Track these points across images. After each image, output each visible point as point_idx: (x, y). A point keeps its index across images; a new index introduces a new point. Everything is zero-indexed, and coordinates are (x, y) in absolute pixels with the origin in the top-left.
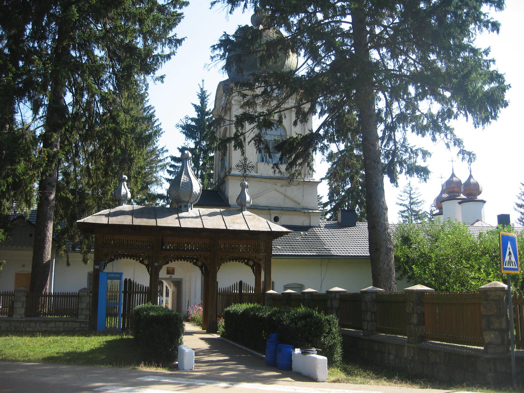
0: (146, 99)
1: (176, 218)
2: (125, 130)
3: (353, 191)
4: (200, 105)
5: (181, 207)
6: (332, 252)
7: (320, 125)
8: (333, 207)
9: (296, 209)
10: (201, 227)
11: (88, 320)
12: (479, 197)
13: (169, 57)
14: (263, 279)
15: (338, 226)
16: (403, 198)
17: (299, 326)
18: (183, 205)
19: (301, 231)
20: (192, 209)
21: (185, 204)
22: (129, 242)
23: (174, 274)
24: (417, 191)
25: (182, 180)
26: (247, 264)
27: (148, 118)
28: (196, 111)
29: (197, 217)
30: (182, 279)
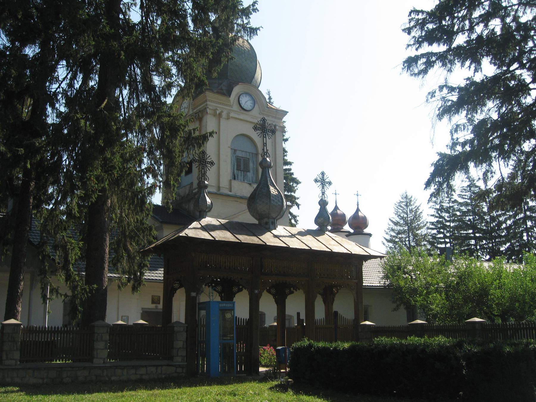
12: (366, 231)
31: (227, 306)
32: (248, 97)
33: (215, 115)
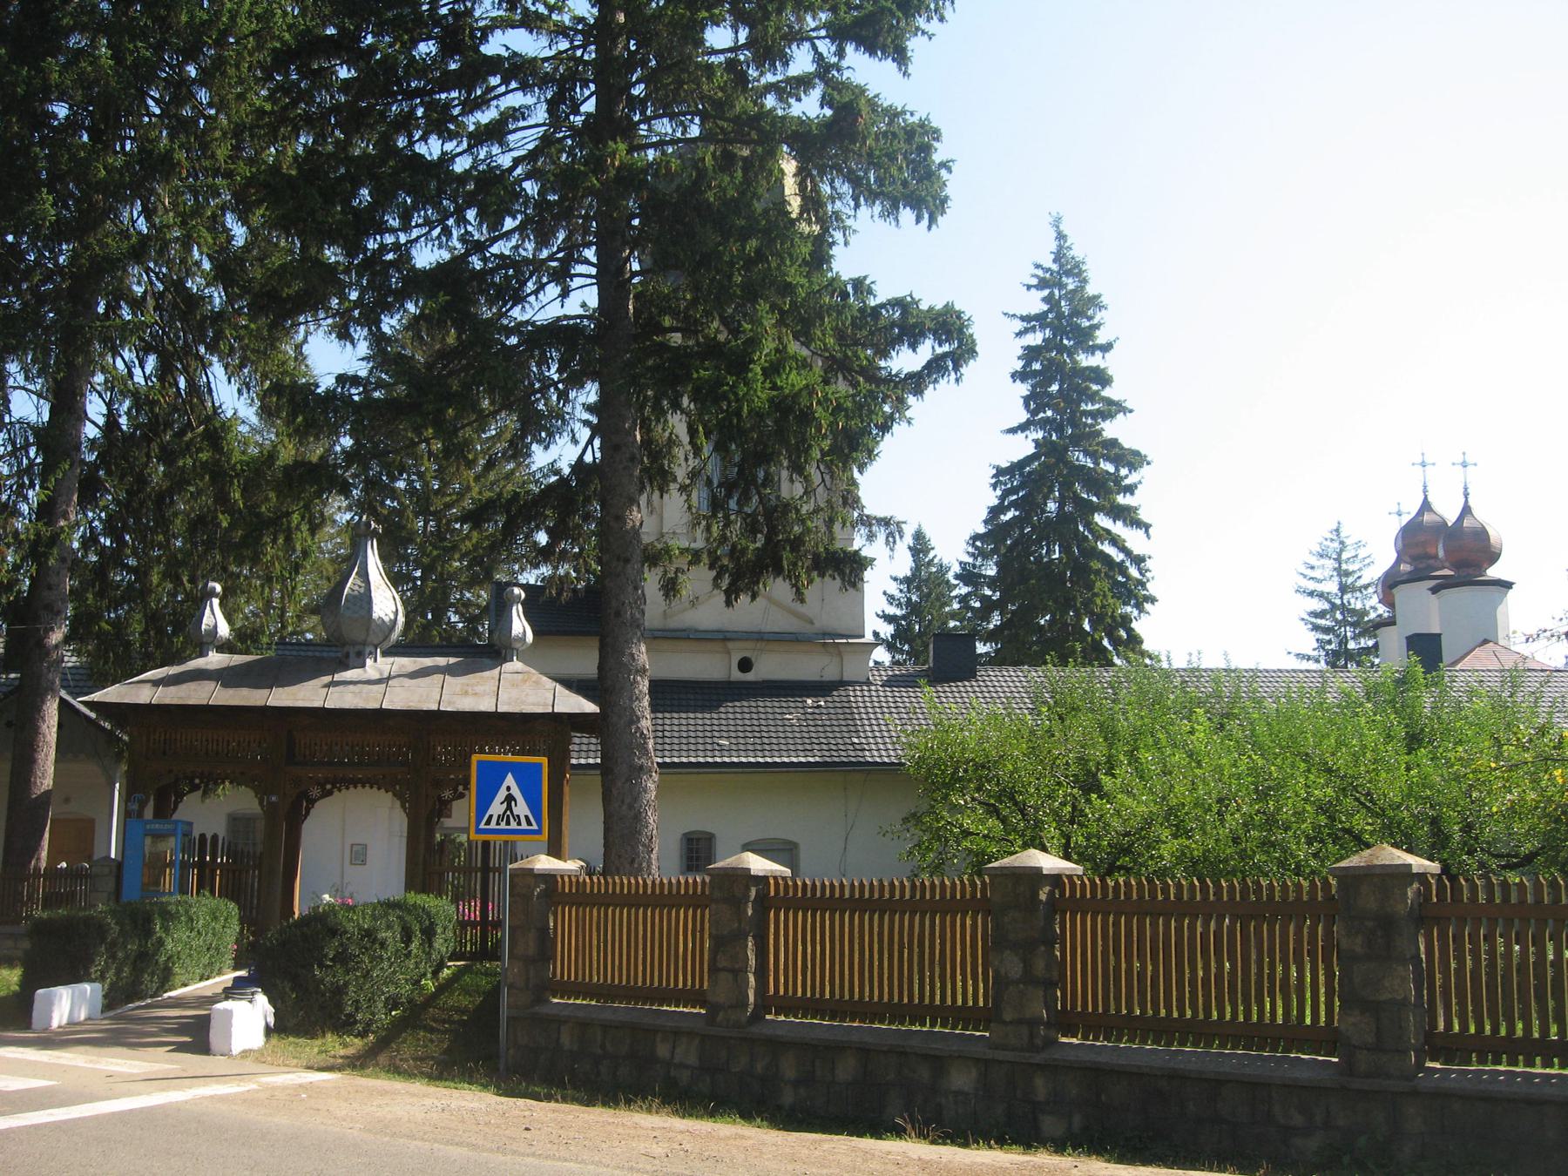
2: (239, 466)
5: (347, 655)
12: (1493, 572)
16: (1317, 574)
19: (808, 697)
21: (358, 648)
24: (1362, 553)
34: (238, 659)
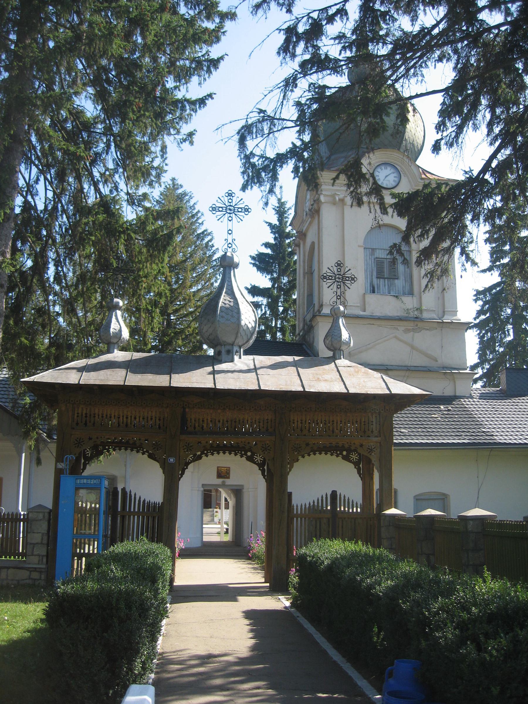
0: (200, 221)
1: (210, 373)
3: (518, 344)
4: (277, 223)
6: (496, 437)
7: (487, 158)
8: (485, 371)
9: (430, 369)
10: (256, 387)
11: (44, 566)
13: (202, 102)
14: (376, 486)
15: (502, 395)
17: (491, 655)
18: (223, 350)
19: (440, 404)
20: (240, 358)
21: (228, 347)
22: (121, 418)
23: (229, 478)
25: (220, 304)
26: (346, 458)
27: (173, 211)
28: (271, 233)
29: (249, 371)
30: (242, 486)
31: (89, 482)
32: (389, 168)
33: (334, 203)
34: (138, 355)
